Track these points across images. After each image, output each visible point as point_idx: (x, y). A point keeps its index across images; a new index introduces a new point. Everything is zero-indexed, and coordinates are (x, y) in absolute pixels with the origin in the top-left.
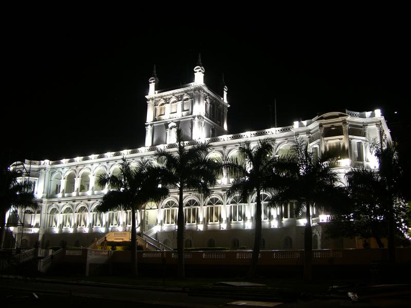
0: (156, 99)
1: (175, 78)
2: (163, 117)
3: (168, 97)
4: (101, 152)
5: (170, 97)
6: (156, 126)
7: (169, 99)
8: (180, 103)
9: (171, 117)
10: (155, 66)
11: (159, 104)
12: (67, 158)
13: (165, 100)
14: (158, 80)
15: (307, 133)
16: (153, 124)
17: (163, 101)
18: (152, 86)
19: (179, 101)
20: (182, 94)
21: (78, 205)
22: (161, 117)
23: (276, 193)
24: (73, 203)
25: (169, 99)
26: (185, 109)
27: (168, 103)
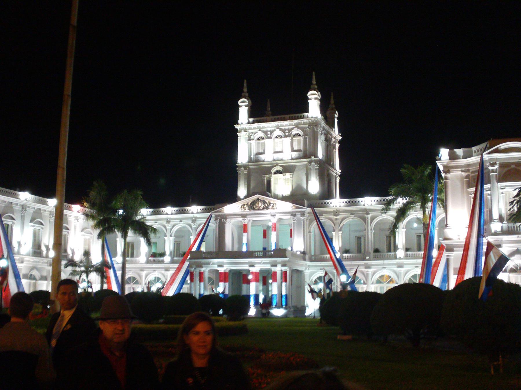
0: (251, 131)
1: (279, 104)
2: (262, 157)
3: (287, 128)
4: (181, 202)
5: (254, 131)
6: (254, 169)
7: (272, 132)
8: (288, 140)
9: (275, 158)
10: (245, 81)
11: (256, 138)
12: (174, 206)
13: (265, 132)
14: (251, 102)
15: (242, 217)
16: (248, 165)
17: (261, 134)
18: (244, 111)
19: (286, 136)
20: (291, 127)
21: (407, 272)
22: (261, 156)
23: (227, 292)
24: (399, 269)
25: (272, 132)
26: (295, 149)
27: (270, 138)
